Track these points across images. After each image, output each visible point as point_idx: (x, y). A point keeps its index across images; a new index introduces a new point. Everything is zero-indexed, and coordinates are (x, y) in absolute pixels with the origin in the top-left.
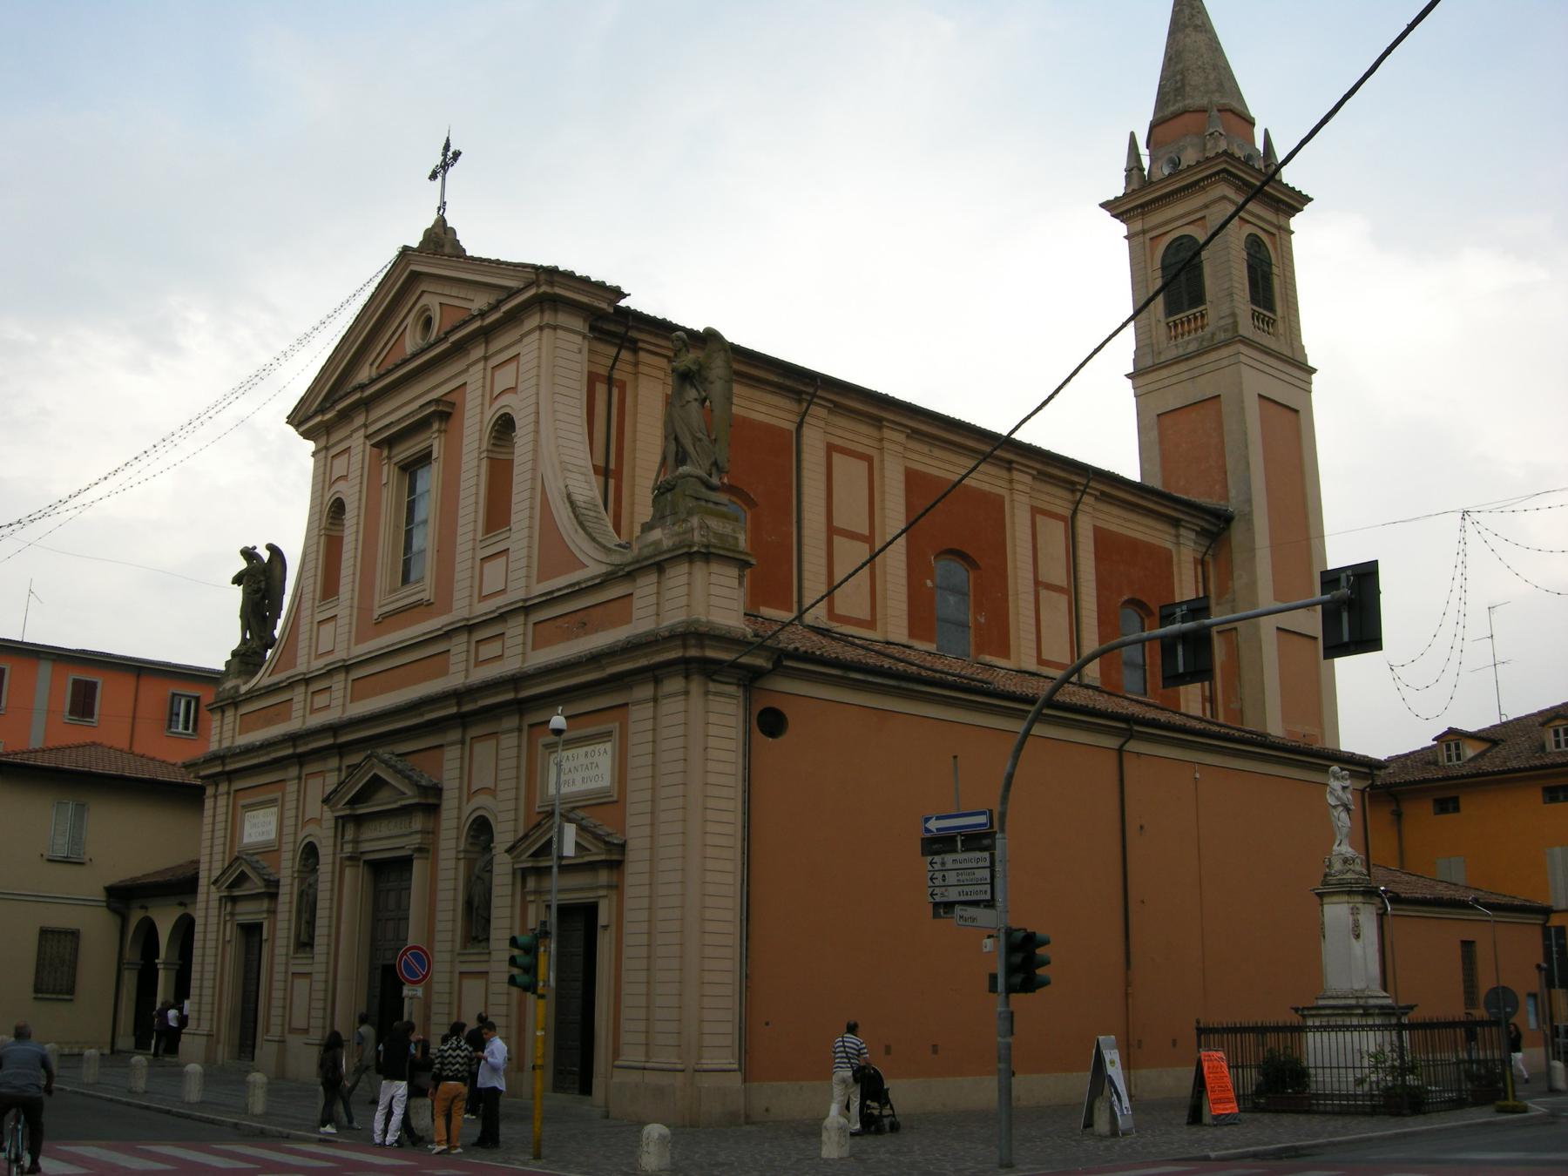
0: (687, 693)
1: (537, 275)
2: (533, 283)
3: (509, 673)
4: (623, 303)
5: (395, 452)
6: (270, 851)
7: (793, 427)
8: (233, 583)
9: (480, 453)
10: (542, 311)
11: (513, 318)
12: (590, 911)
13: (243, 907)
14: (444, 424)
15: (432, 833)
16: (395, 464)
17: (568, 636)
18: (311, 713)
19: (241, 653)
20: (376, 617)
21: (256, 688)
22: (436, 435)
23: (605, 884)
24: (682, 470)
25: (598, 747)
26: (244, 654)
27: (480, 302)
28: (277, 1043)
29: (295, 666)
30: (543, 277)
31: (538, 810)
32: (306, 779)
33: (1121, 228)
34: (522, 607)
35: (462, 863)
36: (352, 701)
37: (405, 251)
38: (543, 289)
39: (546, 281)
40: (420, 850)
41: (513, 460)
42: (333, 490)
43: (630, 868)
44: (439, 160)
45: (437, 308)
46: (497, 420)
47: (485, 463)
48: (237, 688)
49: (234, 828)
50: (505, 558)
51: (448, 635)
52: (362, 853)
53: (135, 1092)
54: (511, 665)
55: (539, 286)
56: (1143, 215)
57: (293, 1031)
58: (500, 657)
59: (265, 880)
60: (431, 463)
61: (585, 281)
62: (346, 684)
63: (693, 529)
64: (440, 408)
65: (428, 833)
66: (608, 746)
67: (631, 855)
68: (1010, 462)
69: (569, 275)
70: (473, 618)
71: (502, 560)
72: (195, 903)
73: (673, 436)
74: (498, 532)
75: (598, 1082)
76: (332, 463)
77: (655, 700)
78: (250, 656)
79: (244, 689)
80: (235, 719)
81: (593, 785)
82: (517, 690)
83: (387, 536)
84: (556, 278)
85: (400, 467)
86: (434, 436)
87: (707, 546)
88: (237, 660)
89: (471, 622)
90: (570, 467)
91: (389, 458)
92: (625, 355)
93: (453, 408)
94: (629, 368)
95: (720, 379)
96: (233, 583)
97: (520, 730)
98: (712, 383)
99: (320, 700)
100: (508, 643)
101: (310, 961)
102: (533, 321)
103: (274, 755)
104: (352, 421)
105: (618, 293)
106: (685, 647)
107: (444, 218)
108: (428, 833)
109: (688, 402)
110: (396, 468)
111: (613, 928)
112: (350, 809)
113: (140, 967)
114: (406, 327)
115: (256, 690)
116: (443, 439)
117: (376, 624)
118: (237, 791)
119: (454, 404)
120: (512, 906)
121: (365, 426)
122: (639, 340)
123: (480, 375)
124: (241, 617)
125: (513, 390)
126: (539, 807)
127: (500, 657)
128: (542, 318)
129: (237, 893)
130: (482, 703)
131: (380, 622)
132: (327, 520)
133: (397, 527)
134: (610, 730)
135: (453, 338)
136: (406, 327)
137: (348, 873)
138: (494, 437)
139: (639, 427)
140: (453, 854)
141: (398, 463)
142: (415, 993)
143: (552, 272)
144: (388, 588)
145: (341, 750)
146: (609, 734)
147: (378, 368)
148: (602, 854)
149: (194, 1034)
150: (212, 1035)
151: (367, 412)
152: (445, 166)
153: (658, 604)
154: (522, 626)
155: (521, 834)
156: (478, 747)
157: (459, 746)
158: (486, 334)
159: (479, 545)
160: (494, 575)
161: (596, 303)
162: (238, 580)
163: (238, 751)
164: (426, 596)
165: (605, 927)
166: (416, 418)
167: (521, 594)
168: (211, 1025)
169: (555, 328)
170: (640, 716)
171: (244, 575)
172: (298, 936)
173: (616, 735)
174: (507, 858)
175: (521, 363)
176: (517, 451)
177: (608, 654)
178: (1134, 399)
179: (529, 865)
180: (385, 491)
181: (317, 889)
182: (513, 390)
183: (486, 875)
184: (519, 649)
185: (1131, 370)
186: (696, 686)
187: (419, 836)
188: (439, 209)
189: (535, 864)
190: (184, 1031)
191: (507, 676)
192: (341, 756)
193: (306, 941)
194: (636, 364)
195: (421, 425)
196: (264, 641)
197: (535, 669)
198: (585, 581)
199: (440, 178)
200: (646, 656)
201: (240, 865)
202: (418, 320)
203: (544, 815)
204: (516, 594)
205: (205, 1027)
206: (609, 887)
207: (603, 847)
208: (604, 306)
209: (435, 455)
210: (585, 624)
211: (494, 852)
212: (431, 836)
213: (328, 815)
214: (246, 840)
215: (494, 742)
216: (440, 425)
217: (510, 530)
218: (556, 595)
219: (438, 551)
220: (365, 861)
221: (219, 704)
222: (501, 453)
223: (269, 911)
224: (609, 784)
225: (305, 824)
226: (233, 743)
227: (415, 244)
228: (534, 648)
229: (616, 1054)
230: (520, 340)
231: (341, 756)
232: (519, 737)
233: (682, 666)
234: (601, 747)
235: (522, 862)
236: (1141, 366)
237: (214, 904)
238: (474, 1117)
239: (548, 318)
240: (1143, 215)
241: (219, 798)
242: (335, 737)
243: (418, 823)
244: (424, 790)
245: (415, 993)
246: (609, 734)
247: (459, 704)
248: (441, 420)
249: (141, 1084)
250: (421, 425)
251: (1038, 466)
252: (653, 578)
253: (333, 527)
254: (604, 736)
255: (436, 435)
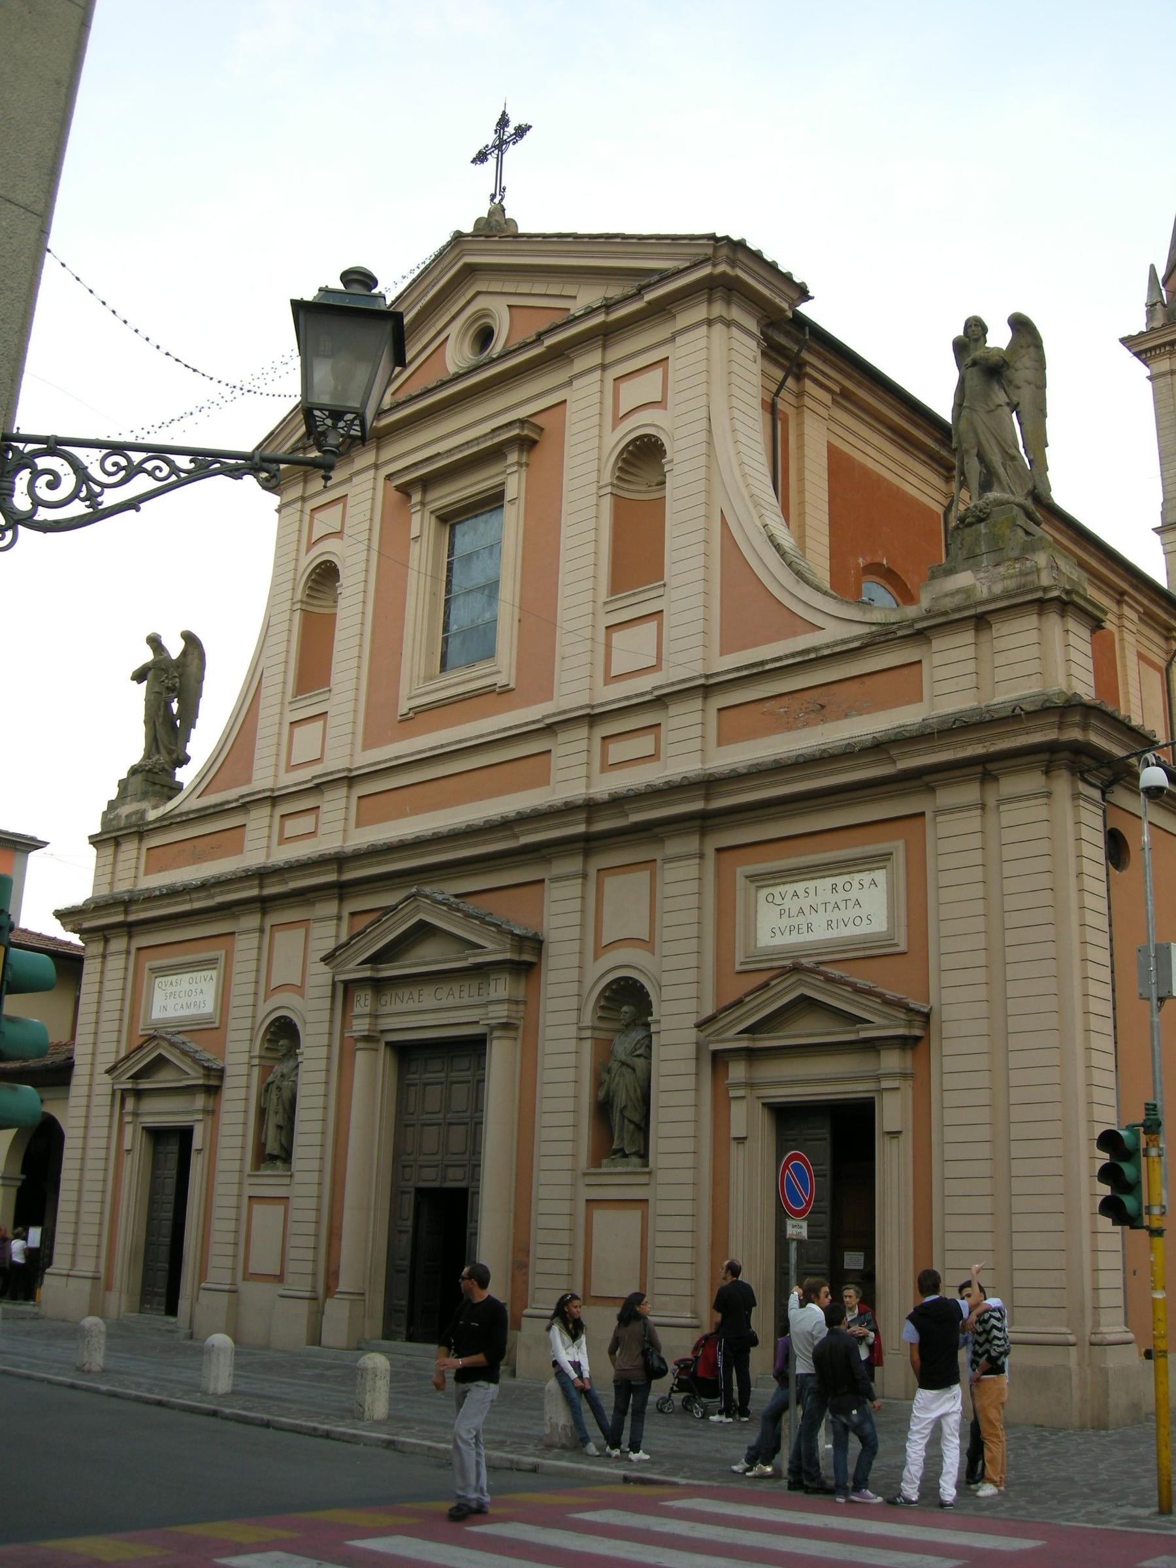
0: (1049, 795)
1: (716, 248)
2: (708, 260)
3: (332, 851)
4: (804, 309)
5: (431, 496)
6: (200, 1028)
7: (940, 510)
8: (133, 679)
9: (293, 604)
10: (710, 301)
11: (662, 310)
12: (185, 1135)
13: (149, 1105)
14: (525, 454)
15: (528, 1004)
16: (432, 512)
17: (788, 724)
18: (280, 843)
19: (147, 768)
20: (405, 711)
21: (176, 812)
22: (515, 468)
23: (898, 1071)
24: (994, 495)
25: (857, 877)
26: (150, 771)
27: (588, 296)
28: (90, 1281)
29: (249, 781)
30: (724, 252)
31: (141, 1033)
32: (271, 932)
33: (1141, 370)
34: (346, 777)
35: (587, 1046)
36: (358, 825)
37: (458, 238)
38: (722, 268)
39: (727, 257)
40: (506, 1026)
41: (334, 616)
42: (316, 551)
43: (227, 1094)
44: (490, 138)
45: (506, 313)
46: (628, 445)
47: (297, 616)
48: (142, 813)
49: (137, 998)
50: (322, 722)
51: (550, 729)
52: (382, 1031)
53: (89, 1372)
54: (329, 843)
55: (714, 265)
56: (1171, 354)
57: (249, 1276)
58: (312, 834)
59: (205, 1068)
60: (502, 506)
61: (772, 267)
62: (348, 802)
63: (1038, 570)
64: (526, 432)
65: (517, 1002)
66: (214, 973)
67: (228, 1082)
68: (1123, 593)
69: (757, 256)
70: (280, 789)
71: (319, 724)
72: (67, 1098)
73: (975, 451)
74: (641, 589)
75: (183, 1305)
76: (312, 518)
77: (104, 956)
78: (156, 773)
79: (152, 815)
80: (348, 802)
81: (864, 929)
82: (707, 798)
83: (420, 605)
84: (741, 256)
85: (437, 517)
86: (509, 471)
87: (1068, 592)
88: (139, 777)
89: (597, 711)
90: (763, 503)
91: (423, 504)
92: (790, 382)
93: (540, 435)
94: (791, 399)
95: (1029, 383)
96: (133, 679)
97: (339, 918)
98: (1019, 388)
99: (294, 827)
100: (324, 818)
101: (286, 1181)
102: (700, 312)
103: (220, 899)
104: (353, 461)
105: (803, 293)
106: (1061, 727)
107: (502, 206)
108: (517, 1002)
109: (1000, 406)
110: (433, 518)
111: (907, 1139)
112: (372, 969)
113: (19, 1183)
114: (447, 338)
115: (172, 817)
116: (524, 474)
117: (401, 721)
118: (139, 949)
119: (542, 429)
120: (110, 1127)
121: (303, 499)
122: (809, 363)
123: (370, 485)
124: (146, 722)
125: (339, 534)
126: (142, 1030)
127: (312, 834)
128: (709, 311)
129: (144, 1085)
130: (636, 818)
131: (412, 718)
132: (304, 591)
133: (434, 594)
134: (890, 851)
135: (549, 341)
136: (447, 338)
137: (361, 1059)
138: (310, 588)
139: (807, 475)
140: (244, 1058)
141: (436, 510)
142: (799, 1230)
143: (740, 246)
144: (422, 675)
145: (342, 890)
146: (886, 857)
147: (393, 394)
148: (199, 1078)
149: (68, 1276)
150: (98, 1278)
151: (378, 449)
152: (500, 145)
153: (269, 837)
154: (345, 799)
155: (123, 1054)
156: (280, 936)
157: (697, 861)
158: (606, 335)
159: (288, 708)
160: (307, 741)
161: (777, 300)
162: (139, 676)
163: (158, 893)
164: (501, 680)
165: (199, 1151)
166: (482, 446)
167: (343, 763)
168: (97, 1266)
169: (729, 324)
170: (246, 946)
171: (150, 669)
172: (260, 1146)
173: (900, 857)
174: (107, 1078)
175: (349, 505)
176: (342, 603)
177: (895, 741)
178: (1163, 558)
179: (129, 1086)
180: (415, 549)
181: (295, 1082)
182: (339, 534)
183: (639, 1063)
184: (340, 825)
185: (1159, 524)
186: (1062, 785)
187: (505, 1006)
188: (493, 197)
189: (135, 1087)
190: (48, 1270)
191: (789, 758)
192: (341, 899)
193: (275, 1153)
194: (800, 395)
195: (492, 455)
196: (174, 756)
197: (321, 855)
198: (828, 646)
199: (492, 160)
200: (980, 741)
201: (158, 1046)
202: (465, 334)
203: (145, 1038)
204: (336, 762)
205: (86, 1266)
206: (904, 1076)
207: (903, 1016)
208: (785, 306)
209: (509, 495)
210: (823, 707)
211: (300, 1059)
212: (521, 1007)
213: (321, 975)
214: (157, 1014)
215: (302, 931)
216: (520, 456)
217: (330, 691)
218: (767, 667)
219: (520, 621)
220: (388, 1044)
221: (114, 834)
222: (627, 490)
223: (206, 1111)
224: (884, 928)
225: (271, 992)
226: (111, 890)
227: (468, 228)
228: (358, 825)
229: (202, 1275)
230: (570, 382)
231: (341, 899)
232: (338, 925)
233: (336, 891)
234: (866, 877)
235: (729, 1040)
236: (1170, 520)
237: (102, 1100)
238: (730, 1420)
239: (718, 309)
240: (1171, 354)
241: (109, 958)
242: (340, 871)
243: (501, 987)
244: (520, 941)
245: (799, 1230)
246: (886, 857)
247: (589, 821)
248: (521, 451)
249: (97, 1359)
250: (492, 455)
251: (1146, 602)
252: (968, 636)
253: (311, 601)
254: (210, 963)
255: (515, 468)
